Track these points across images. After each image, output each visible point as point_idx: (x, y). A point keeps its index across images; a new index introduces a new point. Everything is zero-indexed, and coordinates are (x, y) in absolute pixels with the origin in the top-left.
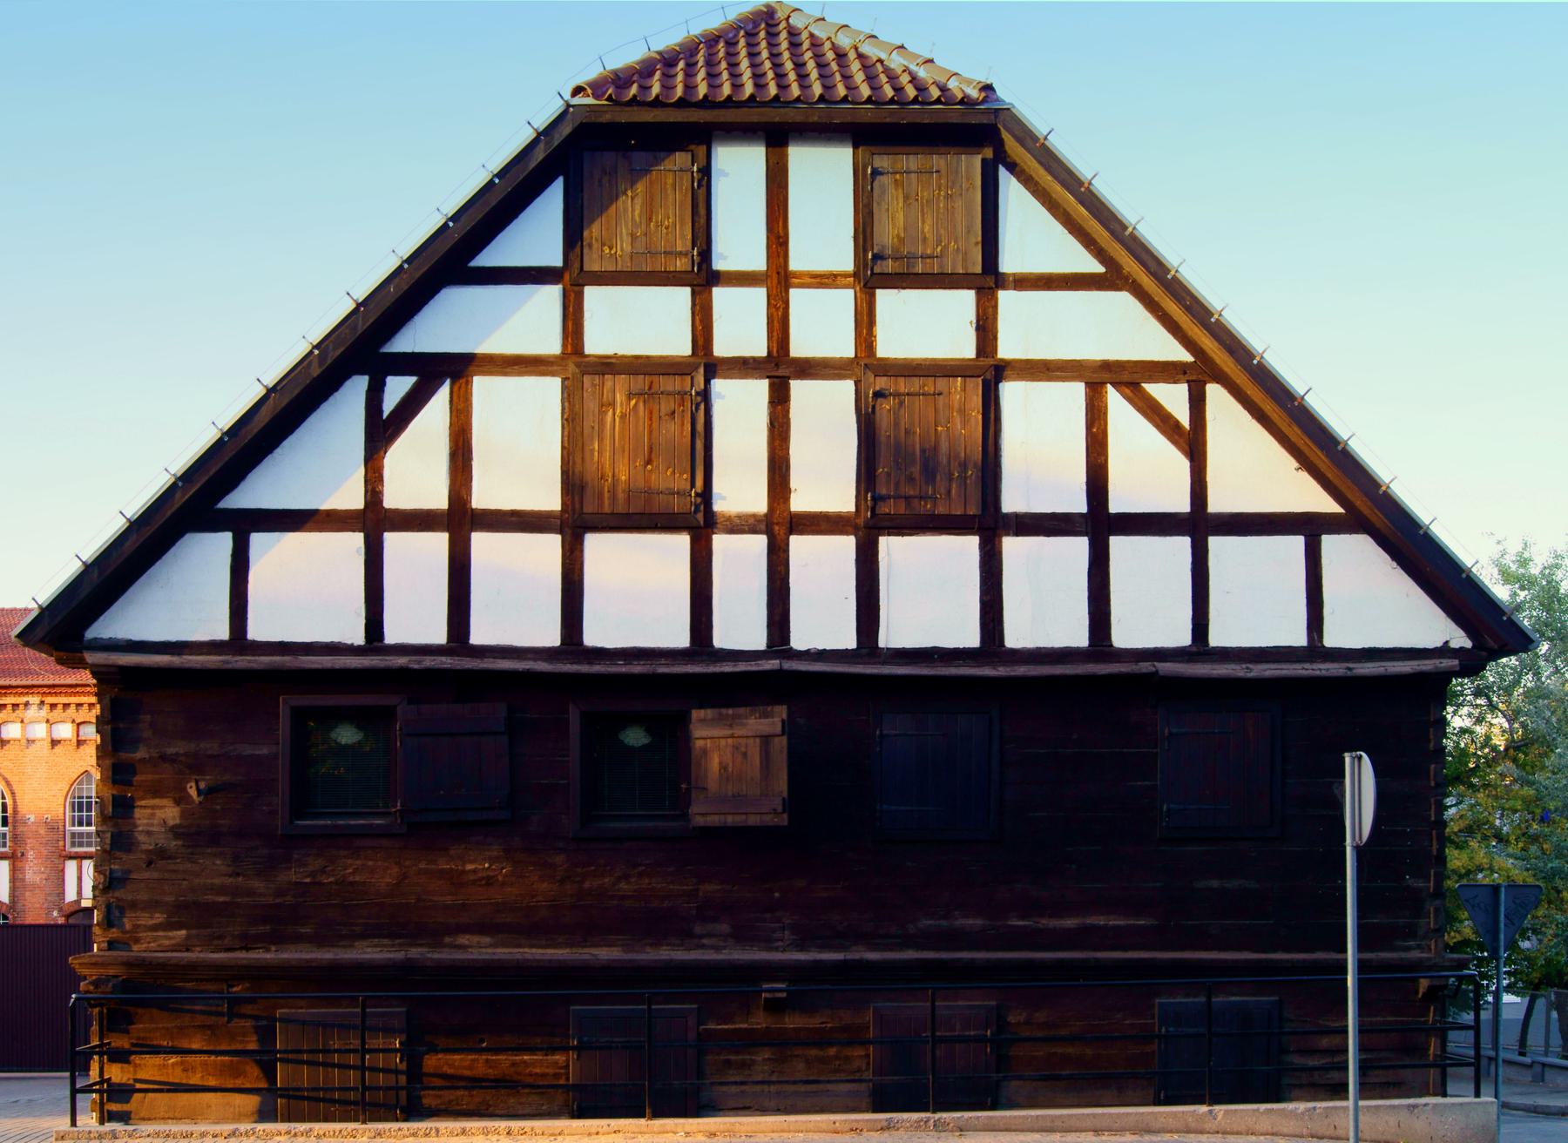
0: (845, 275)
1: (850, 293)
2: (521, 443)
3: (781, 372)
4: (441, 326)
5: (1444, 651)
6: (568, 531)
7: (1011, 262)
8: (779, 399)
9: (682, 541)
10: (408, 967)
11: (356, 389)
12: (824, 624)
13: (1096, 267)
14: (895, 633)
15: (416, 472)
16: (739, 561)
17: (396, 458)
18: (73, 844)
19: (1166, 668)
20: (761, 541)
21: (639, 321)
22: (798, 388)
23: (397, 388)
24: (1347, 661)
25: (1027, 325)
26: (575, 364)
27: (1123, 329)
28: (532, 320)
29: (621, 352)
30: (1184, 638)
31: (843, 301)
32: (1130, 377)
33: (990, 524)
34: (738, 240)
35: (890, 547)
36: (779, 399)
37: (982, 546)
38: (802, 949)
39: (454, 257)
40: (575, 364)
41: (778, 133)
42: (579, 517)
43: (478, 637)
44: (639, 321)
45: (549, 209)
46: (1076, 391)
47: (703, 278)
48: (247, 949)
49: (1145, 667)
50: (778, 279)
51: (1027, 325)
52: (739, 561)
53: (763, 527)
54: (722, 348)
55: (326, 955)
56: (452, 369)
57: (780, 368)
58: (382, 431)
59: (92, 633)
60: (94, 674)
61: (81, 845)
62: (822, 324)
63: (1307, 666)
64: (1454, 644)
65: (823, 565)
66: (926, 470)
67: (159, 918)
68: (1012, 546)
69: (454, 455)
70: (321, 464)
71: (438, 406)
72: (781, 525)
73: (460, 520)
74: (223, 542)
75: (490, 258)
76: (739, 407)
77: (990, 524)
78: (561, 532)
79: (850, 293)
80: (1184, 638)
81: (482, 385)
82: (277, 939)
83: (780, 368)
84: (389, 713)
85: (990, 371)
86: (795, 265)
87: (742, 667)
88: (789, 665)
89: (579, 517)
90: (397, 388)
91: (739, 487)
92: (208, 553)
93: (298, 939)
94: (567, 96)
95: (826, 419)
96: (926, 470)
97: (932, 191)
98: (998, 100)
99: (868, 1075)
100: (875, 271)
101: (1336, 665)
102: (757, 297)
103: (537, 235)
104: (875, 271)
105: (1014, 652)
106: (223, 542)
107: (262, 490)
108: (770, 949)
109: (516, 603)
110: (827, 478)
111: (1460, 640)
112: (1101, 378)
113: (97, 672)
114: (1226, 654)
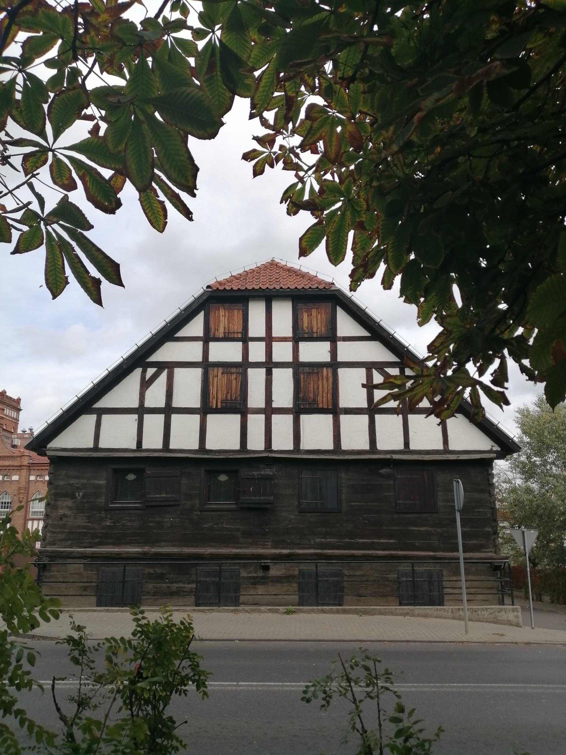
0: (290, 338)
1: (291, 343)
2: (189, 388)
3: (270, 366)
4: (168, 352)
5: (490, 451)
6: (201, 413)
7: (340, 333)
8: (269, 374)
9: (238, 417)
10: (145, 553)
11: (138, 372)
12: (283, 441)
13: (367, 334)
14: (305, 445)
15: (156, 396)
16: (256, 423)
17: (149, 393)
18: (32, 515)
19: (396, 457)
20: (263, 416)
21: (226, 352)
22: (275, 371)
23: (151, 371)
24: (458, 454)
25: (346, 351)
26: (206, 365)
27: (375, 352)
28: (193, 351)
29: (220, 361)
30: (401, 447)
31: (289, 345)
32: (380, 366)
33: (335, 410)
34: (257, 327)
35: (304, 418)
36: (269, 374)
37: (333, 418)
38: (274, 548)
39: (169, 333)
40: (206, 365)
41: (269, 297)
42: (206, 409)
43: (172, 446)
44: (226, 352)
45: (200, 319)
46: (363, 371)
47: (245, 339)
48: (91, 547)
49: (388, 456)
50: (269, 339)
51: (346, 351)
52: (256, 423)
53: (263, 412)
54: (252, 359)
55: (116, 550)
56: (161, 366)
57: (269, 365)
58: (145, 384)
59: (49, 446)
60: (49, 459)
61: (34, 515)
62: (282, 352)
63: (444, 456)
64: (494, 449)
65: (282, 425)
66: (315, 392)
67: (63, 536)
68: (344, 418)
69: (167, 391)
70: (126, 393)
71: (164, 376)
72: (269, 411)
73: (168, 410)
74: (94, 417)
75: (180, 334)
76: (256, 377)
77: (335, 410)
78: (199, 414)
79: (291, 343)
80: (401, 447)
81: (178, 372)
82: (100, 544)
83: (269, 365)
84: (143, 470)
85: (334, 365)
86: (274, 335)
87: (256, 455)
88: (271, 455)
89: (206, 409)
90: (151, 371)
91: (256, 399)
92: (87, 421)
93: (109, 544)
94: (205, 288)
95: (284, 381)
96: (315, 392)
97: (315, 319)
98: (336, 287)
99: (297, 593)
100: (299, 336)
101: (454, 456)
102: (262, 345)
103: (196, 327)
104: (299, 336)
105: (344, 451)
106: (94, 417)
107: (105, 402)
108: (264, 548)
109: (185, 435)
110: (284, 396)
111: (497, 448)
112: (369, 366)
113: (50, 458)
114: (211, 451)
